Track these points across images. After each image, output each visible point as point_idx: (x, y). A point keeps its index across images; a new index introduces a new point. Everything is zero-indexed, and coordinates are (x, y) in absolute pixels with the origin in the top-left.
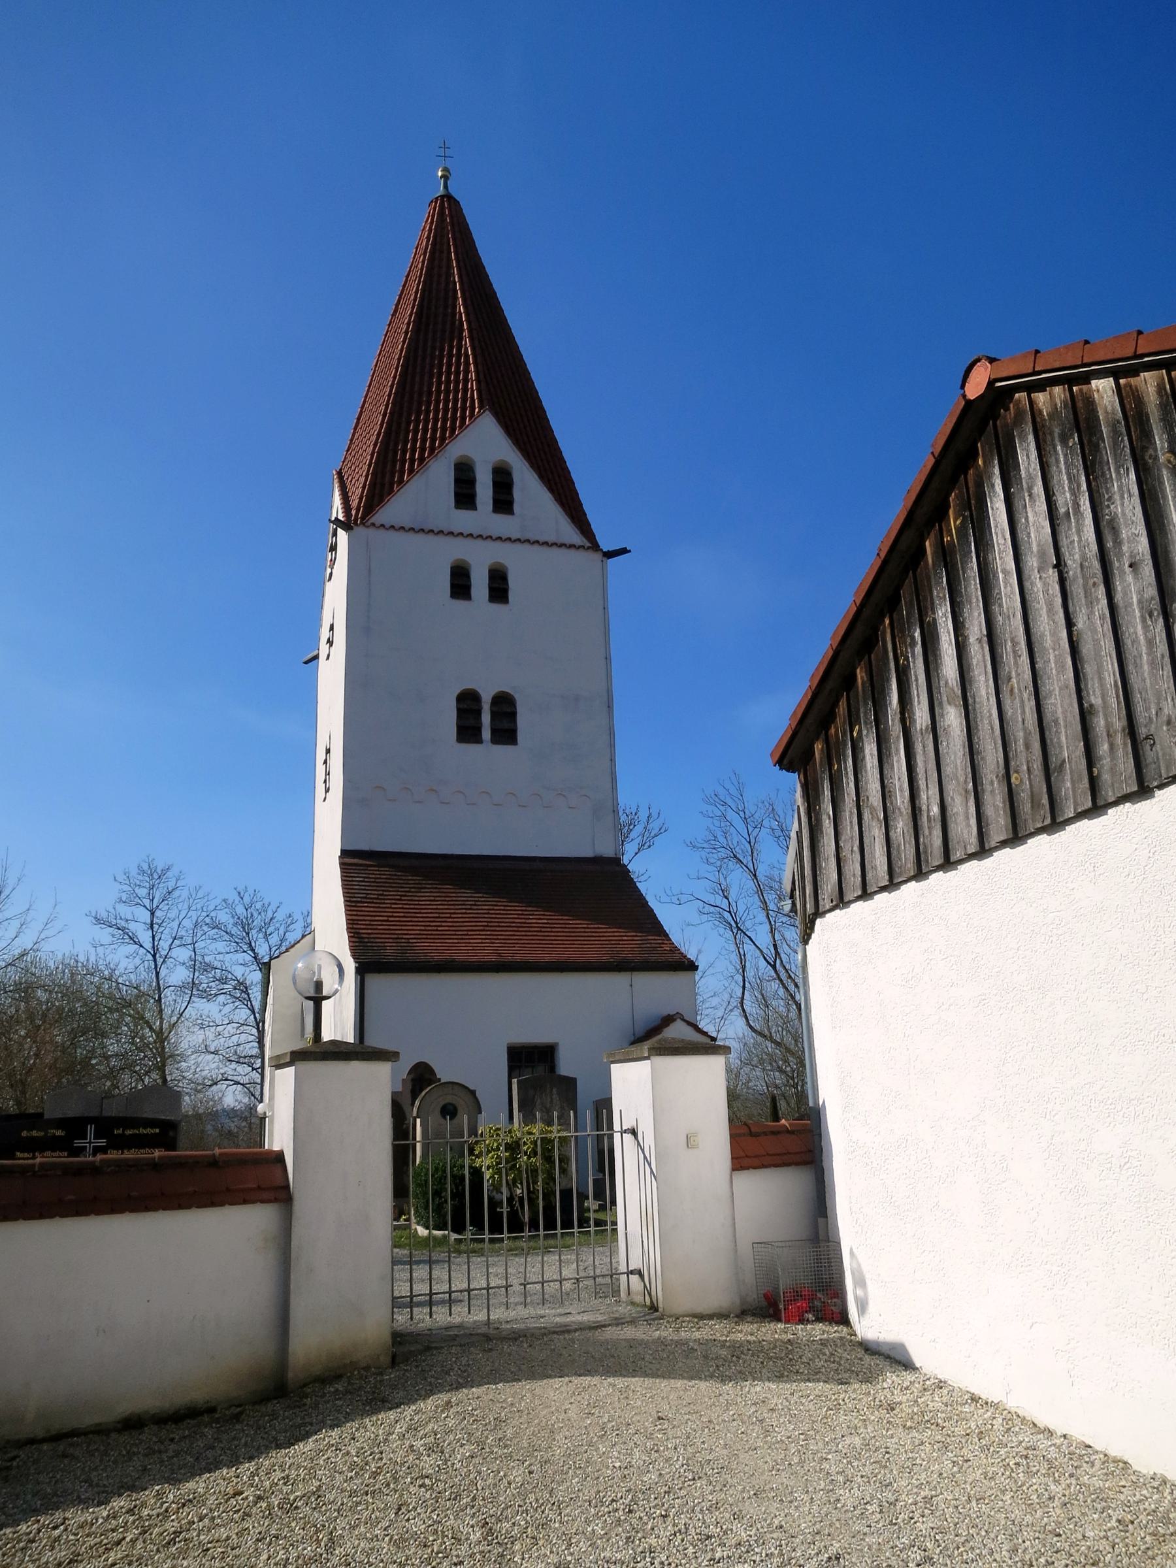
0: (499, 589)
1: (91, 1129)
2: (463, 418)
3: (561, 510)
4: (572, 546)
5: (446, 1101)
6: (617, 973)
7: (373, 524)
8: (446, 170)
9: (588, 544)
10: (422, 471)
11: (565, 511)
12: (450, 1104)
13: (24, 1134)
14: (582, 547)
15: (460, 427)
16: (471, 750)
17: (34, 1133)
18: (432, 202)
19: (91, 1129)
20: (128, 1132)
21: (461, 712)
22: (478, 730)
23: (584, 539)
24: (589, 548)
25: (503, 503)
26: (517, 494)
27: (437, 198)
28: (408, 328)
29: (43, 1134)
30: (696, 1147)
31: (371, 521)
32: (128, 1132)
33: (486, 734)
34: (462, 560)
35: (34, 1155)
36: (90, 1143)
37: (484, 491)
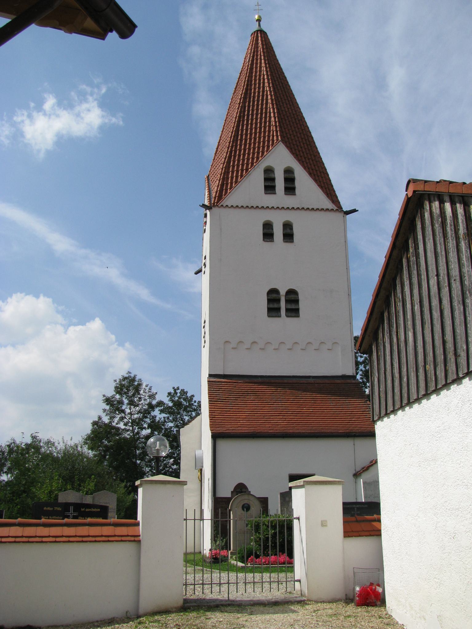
0: (288, 236)
1: (71, 508)
2: (268, 147)
3: (321, 191)
4: (327, 210)
5: (245, 503)
6: (222, 439)
7: (222, 206)
8: (260, 17)
9: (335, 208)
10: (247, 175)
11: (323, 191)
12: (247, 504)
13: (45, 508)
14: (332, 210)
15: (267, 151)
16: (275, 321)
17: (49, 508)
18: (252, 34)
19: (71, 508)
20: (87, 510)
21: (269, 301)
22: (279, 309)
23: (334, 206)
24: (337, 210)
25: (290, 189)
26: (297, 184)
27: (255, 32)
28: (240, 101)
29: (52, 509)
30: (326, 526)
31: (221, 204)
32: (87, 510)
33: (283, 312)
34: (266, 221)
35: (49, 517)
36: (71, 514)
37: (280, 184)
